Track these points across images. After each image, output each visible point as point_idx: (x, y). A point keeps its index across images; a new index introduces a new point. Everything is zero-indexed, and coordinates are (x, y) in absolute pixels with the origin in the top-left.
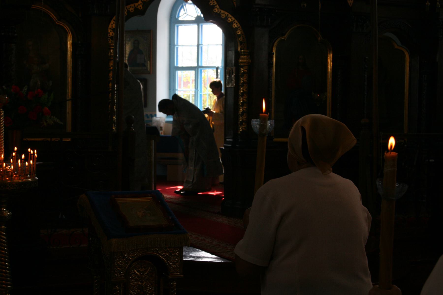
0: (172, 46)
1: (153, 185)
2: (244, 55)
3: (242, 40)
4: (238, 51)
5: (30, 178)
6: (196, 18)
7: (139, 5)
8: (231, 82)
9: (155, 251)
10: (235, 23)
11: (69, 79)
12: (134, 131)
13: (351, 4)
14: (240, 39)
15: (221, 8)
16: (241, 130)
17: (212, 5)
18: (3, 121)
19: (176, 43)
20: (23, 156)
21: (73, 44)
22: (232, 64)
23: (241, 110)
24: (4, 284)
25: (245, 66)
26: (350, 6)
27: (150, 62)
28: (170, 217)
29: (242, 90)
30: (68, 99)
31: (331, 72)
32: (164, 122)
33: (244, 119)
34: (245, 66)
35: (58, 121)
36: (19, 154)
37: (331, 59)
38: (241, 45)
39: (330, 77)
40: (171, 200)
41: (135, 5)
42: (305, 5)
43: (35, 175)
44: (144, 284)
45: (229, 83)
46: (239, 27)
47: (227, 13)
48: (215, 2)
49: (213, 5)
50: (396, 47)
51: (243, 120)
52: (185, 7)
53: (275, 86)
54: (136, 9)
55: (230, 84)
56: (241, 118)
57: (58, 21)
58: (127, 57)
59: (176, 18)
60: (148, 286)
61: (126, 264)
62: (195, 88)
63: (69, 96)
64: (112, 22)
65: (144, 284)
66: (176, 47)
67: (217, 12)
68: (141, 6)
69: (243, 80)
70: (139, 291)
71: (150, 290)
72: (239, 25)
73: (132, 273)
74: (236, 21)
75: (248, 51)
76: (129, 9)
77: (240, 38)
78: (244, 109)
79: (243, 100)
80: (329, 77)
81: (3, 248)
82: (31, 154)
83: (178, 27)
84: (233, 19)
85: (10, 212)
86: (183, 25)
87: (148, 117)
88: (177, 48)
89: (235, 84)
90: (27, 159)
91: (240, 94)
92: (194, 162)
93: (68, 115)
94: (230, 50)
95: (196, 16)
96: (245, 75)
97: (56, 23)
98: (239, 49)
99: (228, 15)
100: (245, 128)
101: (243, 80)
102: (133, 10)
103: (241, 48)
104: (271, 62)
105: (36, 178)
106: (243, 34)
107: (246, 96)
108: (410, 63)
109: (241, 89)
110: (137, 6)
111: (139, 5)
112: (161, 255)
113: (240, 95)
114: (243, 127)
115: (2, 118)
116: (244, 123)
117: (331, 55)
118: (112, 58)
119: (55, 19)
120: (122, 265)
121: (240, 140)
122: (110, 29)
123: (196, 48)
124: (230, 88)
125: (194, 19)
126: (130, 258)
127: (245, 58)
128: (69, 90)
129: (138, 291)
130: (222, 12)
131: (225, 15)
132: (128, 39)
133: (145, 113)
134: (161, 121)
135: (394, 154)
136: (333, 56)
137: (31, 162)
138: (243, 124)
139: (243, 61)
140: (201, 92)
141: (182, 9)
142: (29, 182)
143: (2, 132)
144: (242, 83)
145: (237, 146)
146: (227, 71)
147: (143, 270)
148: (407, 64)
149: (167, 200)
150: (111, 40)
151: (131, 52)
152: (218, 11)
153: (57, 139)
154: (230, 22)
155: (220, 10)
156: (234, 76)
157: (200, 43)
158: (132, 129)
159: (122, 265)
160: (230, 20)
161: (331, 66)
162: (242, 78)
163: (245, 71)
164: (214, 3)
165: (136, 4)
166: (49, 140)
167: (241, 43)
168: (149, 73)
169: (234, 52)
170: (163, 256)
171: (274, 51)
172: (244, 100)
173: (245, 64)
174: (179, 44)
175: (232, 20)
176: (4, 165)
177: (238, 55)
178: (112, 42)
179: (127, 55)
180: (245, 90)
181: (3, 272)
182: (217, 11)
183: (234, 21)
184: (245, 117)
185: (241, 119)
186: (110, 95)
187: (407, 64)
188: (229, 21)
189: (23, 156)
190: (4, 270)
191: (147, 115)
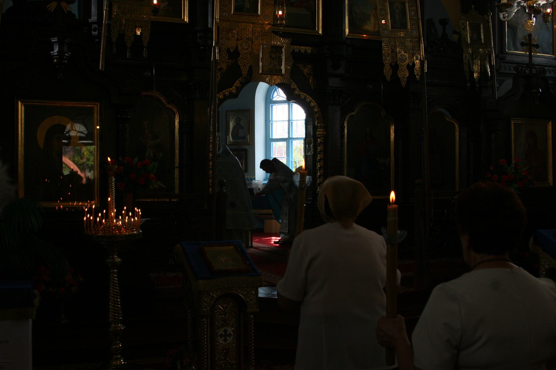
1: (250, 236)
2: (320, 128)
3: (318, 116)
5: (135, 231)
7: (233, 89)
8: (310, 151)
9: (235, 291)
10: (312, 102)
13: (404, 85)
14: (317, 115)
17: (293, 88)
18: (114, 186)
19: (271, 120)
20: (130, 214)
21: (180, 123)
22: (311, 136)
24: (117, 316)
26: (404, 87)
31: (393, 141)
32: (261, 184)
35: (162, 185)
36: (127, 211)
37: (393, 131)
38: (317, 120)
40: (265, 249)
41: (229, 90)
42: (371, 86)
43: (140, 229)
44: (227, 317)
45: (308, 151)
46: (316, 105)
47: (305, 95)
48: (295, 85)
49: (294, 88)
50: (448, 119)
52: (277, 90)
53: (347, 153)
54: (231, 93)
56: (319, 180)
60: (231, 319)
61: (212, 301)
62: (287, 156)
65: (227, 317)
66: (271, 122)
67: (297, 94)
68: (235, 90)
69: (319, 149)
70: (223, 322)
71: (232, 322)
72: (316, 104)
73: (217, 308)
74: (313, 101)
77: (317, 115)
78: (321, 173)
81: (115, 287)
82: (137, 212)
84: (311, 99)
85: (120, 258)
87: (248, 181)
88: (272, 123)
90: (133, 216)
92: (288, 216)
93: (176, 180)
97: (167, 106)
98: (316, 124)
99: (306, 96)
101: (319, 149)
104: (343, 134)
105: (140, 231)
107: (322, 162)
108: (460, 132)
109: (318, 156)
110: (232, 91)
111: (233, 89)
112: (240, 294)
115: (113, 184)
117: (393, 127)
119: (165, 103)
120: (208, 301)
123: (287, 123)
126: (214, 296)
129: (222, 323)
130: (302, 93)
131: (304, 96)
132: (232, 117)
133: (246, 177)
134: (259, 183)
135: (394, 206)
136: (394, 128)
137: (136, 218)
140: (292, 157)
141: (276, 92)
142: (135, 234)
143: (113, 194)
146: (306, 141)
147: (226, 305)
148: (457, 134)
149: (261, 248)
151: (234, 127)
152: (298, 93)
153: (168, 200)
159: (208, 301)
161: (394, 136)
164: (295, 87)
165: (231, 89)
166: (156, 200)
167: (318, 119)
168: (249, 144)
170: (242, 294)
171: (346, 125)
172: (321, 165)
173: (322, 136)
176: (115, 221)
177: (315, 128)
179: (231, 130)
180: (321, 157)
181: (116, 307)
182: (297, 93)
184: (322, 179)
185: (319, 181)
187: (457, 134)
189: (130, 214)
190: (116, 305)
191: (247, 179)
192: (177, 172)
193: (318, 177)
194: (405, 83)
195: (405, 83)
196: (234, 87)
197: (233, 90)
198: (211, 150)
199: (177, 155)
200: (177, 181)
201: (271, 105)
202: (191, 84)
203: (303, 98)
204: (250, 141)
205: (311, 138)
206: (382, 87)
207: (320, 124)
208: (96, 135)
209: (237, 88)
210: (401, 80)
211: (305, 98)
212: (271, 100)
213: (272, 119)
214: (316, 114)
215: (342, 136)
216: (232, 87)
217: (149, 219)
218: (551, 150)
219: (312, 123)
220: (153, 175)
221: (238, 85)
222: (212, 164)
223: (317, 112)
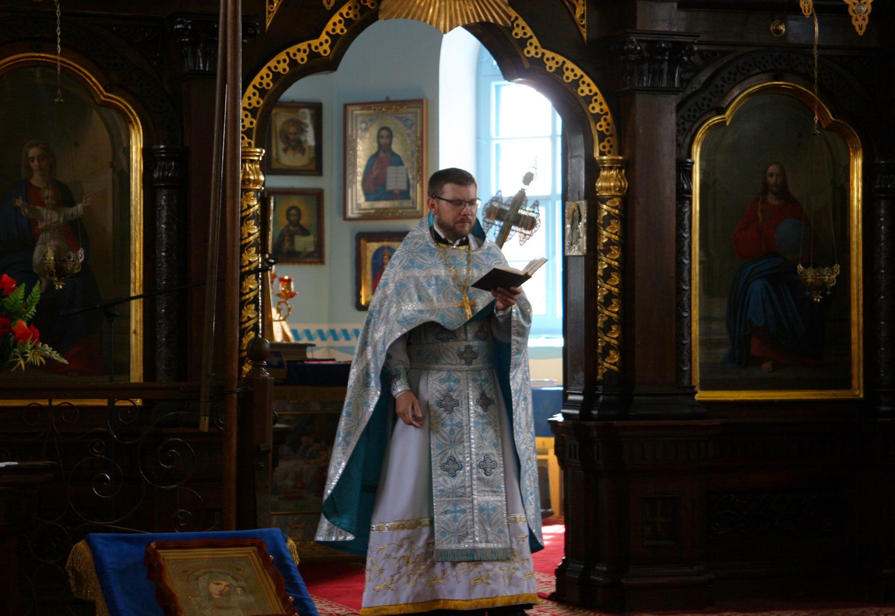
2: (610, 168)
3: (603, 129)
7: (321, 44)
8: (577, 242)
10: (583, 83)
11: (138, 245)
13: (861, 29)
14: (602, 126)
15: (545, 44)
21: (147, 153)
26: (861, 33)
28: (290, 597)
30: (133, 294)
31: (860, 206)
33: (613, 341)
34: (612, 197)
35: (55, 356)
39: (858, 223)
41: (309, 46)
47: (560, 59)
53: (700, 249)
54: (313, 55)
55: (574, 248)
57: (105, 93)
58: (359, 174)
63: (137, 288)
66: (493, 144)
67: (533, 57)
68: (326, 47)
75: (620, 158)
76: (295, 55)
77: (599, 124)
80: (856, 222)
83: (497, 87)
91: (600, 273)
93: (133, 336)
96: (613, 222)
98: (597, 155)
99: (564, 63)
100: (614, 364)
113: (600, 276)
121: (601, 399)
124: (574, 256)
127: (612, 176)
128: (138, 273)
130: (549, 54)
131: (557, 63)
139: (605, 184)
145: (595, 412)
146: (566, 211)
151: (373, 160)
152: (537, 54)
155: (541, 50)
156: (585, 224)
162: (604, 230)
165: (314, 43)
167: (602, 136)
173: (613, 193)
177: (593, 169)
179: (360, 170)
183: (583, 79)
192: (136, 311)
194: (864, 19)
195: (865, 23)
196: (324, 37)
197: (322, 44)
199: (138, 256)
200: (136, 342)
201: (497, 87)
202: (179, 26)
204: (422, 205)
205: (580, 199)
206: (817, 29)
208: (760, 86)
209: (334, 38)
210: (851, 13)
211: (560, 70)
213: (497, 133)
214: (596, 123)
215: (683, 195)
216: (317, 36)
217: (16, 463)
218: (860, 237)
220: (25, 324)
221: (338, 31)
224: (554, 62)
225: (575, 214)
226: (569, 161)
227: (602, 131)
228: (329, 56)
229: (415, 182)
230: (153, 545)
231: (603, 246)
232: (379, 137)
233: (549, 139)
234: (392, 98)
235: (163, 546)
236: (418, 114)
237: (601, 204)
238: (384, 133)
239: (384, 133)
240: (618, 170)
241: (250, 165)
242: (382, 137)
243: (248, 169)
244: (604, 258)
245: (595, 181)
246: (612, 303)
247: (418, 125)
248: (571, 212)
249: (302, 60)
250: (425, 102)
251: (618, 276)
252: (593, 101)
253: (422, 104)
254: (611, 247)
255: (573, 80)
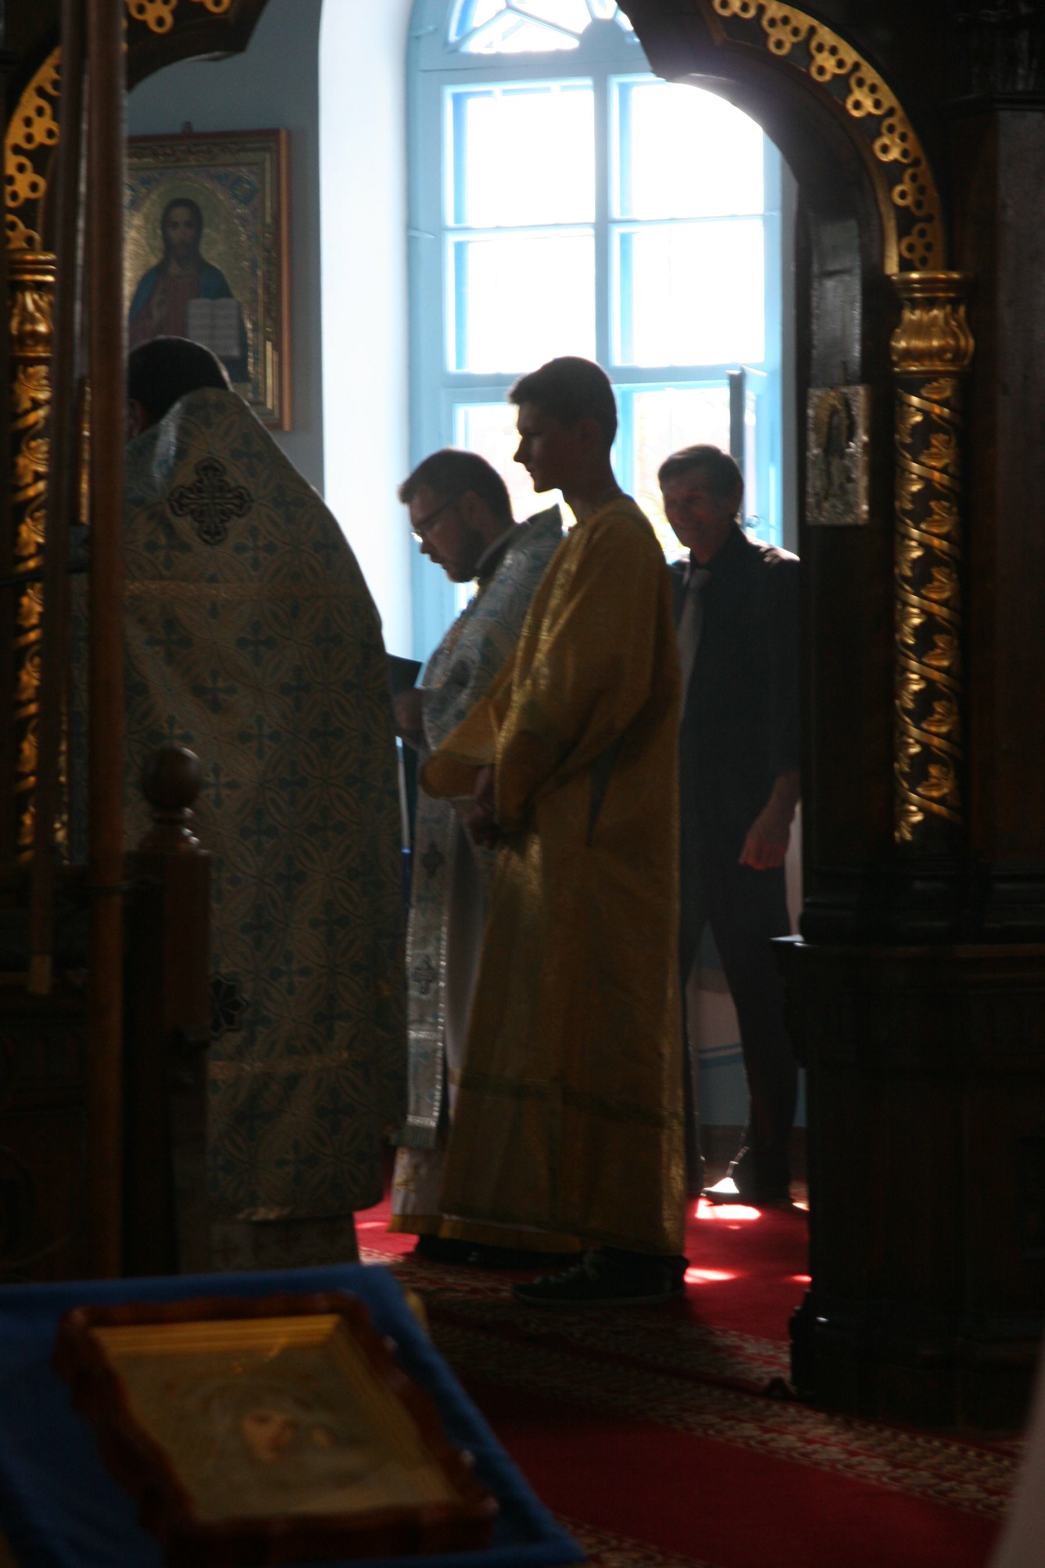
0: (425, 237)
2: (929, 304)
3: (908, 202)
4: (889, 277)
6: (583, 38)
12: (204, 852)
14: (901, 196)
16: (918, 818)
19: (450, 220)
23: (917, 682)
25: (929, 377)
27: (277, 348)
29: (921, 545)
33: (936, 741)
34: (929, 377)
46: (891, 112)
47: (804, 20)
51: (925, 746)
56: (914, 731)
59: (446, 43)
64: (29, 102)
66: (451, 240)
67: (735, 16)
72: (889, 100)
75: (955, 276)
77: (899, 188)
78: (936, 675)
79: (924, 612)
83: (458, 99)
84: (850, 56)
86: (497, 88)
88: (460, 247)
89: (870, 505)
94: (831, 274)
95: (581, 23)
98: (892, 267)
99: (812, 31)
100: (940, 801)
101: (921, 478)
102: (169, 20)
103: (906, 254)
106: (916, 163)
114: (932, 799)
116: (934, 771)
118: (41, 352)
122: (17, 150)
125: (571, 44)
131: (796, 32)
138: (926, 776)
139: (918, 344)
144: (913, 494)
146: (811, 412)
150: (21, 226)
154: (827, 77)
157: (615, 213)
158: (186, 839)
160: (829, 63)
163: (937, 409)
167: (906, 221)
169: (855, 285)
172: (936, 608)
173: (939, 366)
174: (470, 221)
175: (840, 64)
178: (30, 240)
180: (936, 542)
183: (859, 74)
184: (944, 729)
185: (918, 742)
186: (28, 820)
188: (821, 70)
193: (910, 705)
198: (31, 492)
201: (458, 99)
203: (784, 51)
205: (848, 383)
207: (923, 264)
212: (454, 50)
213: (459, 216)
219: (853, 261)
222: (38, 608)
223: (905, 167)
224: (789, 28)
225: (836, 419)
226: (816, 285)
227: (906, 208)
228: (226, 12)
229: (261, 337)
230: (78, 1316)
231: (912, 502)
232: (166, 223)
233: (591, 232)
234: (197, 128)
235: (104, 1319)
236: (268, 165)
237: (906, 395)
238: (181, 214)
239: (181, 214)
240: (949, 308)
241: (36, 297)
242: (175, 225)
243: (30, 306)
244: (915, 532)
245: (890, 335)
246: (935, 646)
247: (268, 191)
248: (824, 416)
249: (160, 22)
250: (283, 136)
251: (949, 577)
252: (884, 130)
253: (278, 142)
254: (933, 504)
255: (835, 76)
